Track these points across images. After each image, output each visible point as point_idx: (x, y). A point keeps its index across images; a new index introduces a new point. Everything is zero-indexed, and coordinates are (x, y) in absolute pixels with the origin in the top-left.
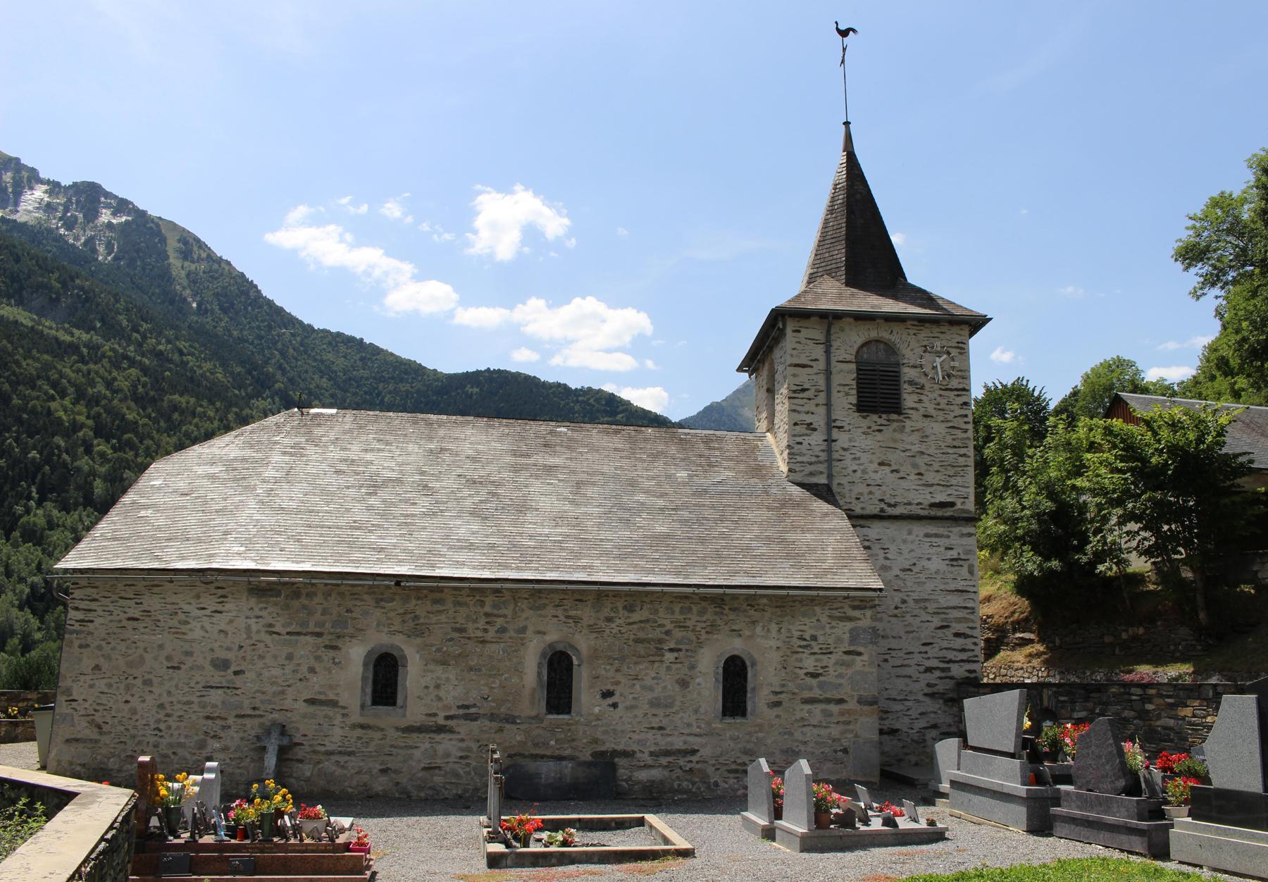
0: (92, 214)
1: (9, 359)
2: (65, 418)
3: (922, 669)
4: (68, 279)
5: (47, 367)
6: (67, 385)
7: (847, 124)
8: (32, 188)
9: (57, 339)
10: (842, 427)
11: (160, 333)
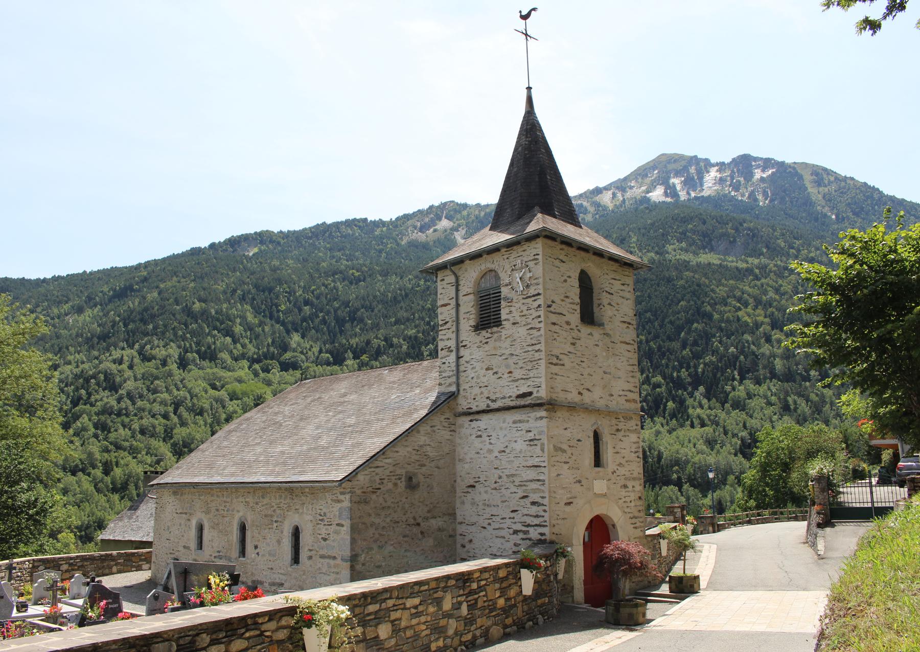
0: (749, 175)
1: (708, 289)
2: (749, 320)
3: (511, 531)
4: (738, 225)
5: (732, 289)
6: (748, 297)
7: (529, 88)
8: (708, 172)
9: (737, 268)
10: (465, 346)
11: (809, 245)
